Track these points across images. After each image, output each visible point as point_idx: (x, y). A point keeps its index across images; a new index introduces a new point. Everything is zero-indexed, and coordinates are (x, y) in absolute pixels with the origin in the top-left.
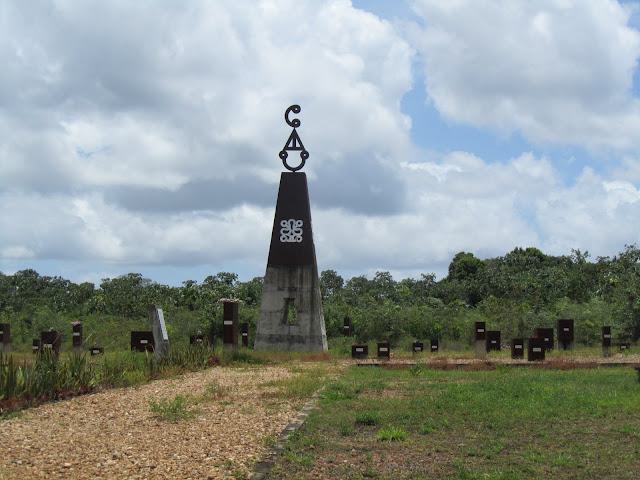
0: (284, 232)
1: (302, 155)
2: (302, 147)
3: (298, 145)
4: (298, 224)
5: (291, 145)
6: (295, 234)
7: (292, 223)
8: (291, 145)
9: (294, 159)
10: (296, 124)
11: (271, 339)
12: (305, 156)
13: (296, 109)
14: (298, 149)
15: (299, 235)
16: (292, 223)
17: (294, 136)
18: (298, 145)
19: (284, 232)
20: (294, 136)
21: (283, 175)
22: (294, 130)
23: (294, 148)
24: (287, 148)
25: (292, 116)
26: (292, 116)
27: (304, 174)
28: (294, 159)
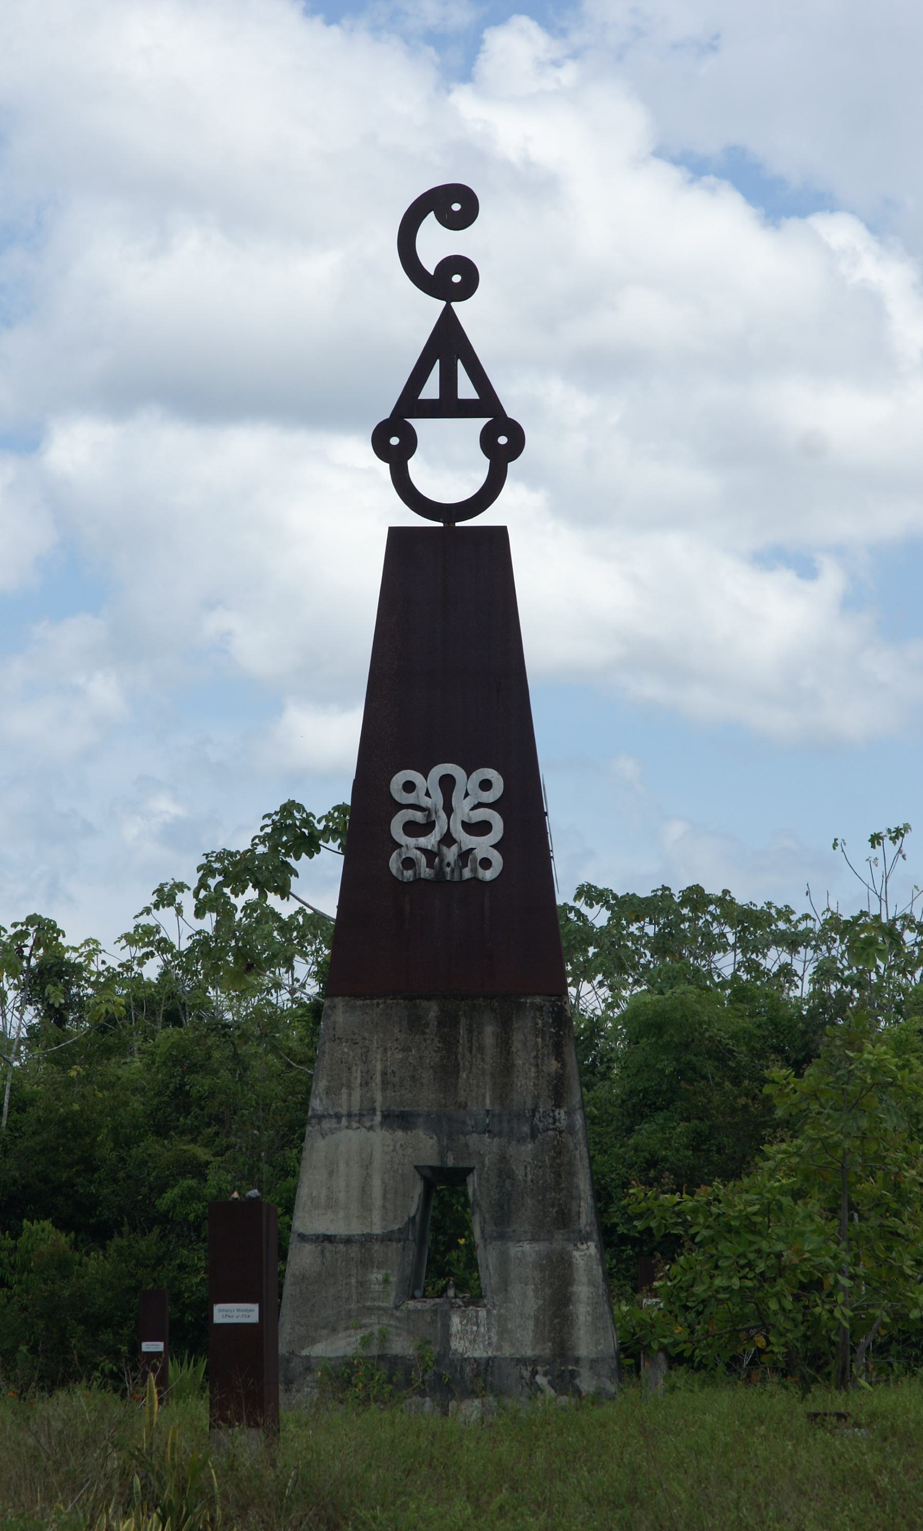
0: (412, 829)
1: (487, 442)
2: (486, 403)
3: (466, 390)
4: (476, 791)
5: (431, 390)
6: (468, 841)
7: (447, 783)
8: (431, 390)
9: (448, 463)
10: (453, 281)
11: (342, 1378)
12: (503, 442)
13: (453, 204)
14: (465, 410)
15: (483, 846)
16: (447, 783)
17: (448, 344)
18: (466, 390)
19: (412, 829)
20: (448, 344)
21: (399, 539)
22: (448, 322)
23: (449, 406)
24: (410, 404)
25: (435, 243)
26: (435, 243)
27: (499, 535)
28: (448, 463)
